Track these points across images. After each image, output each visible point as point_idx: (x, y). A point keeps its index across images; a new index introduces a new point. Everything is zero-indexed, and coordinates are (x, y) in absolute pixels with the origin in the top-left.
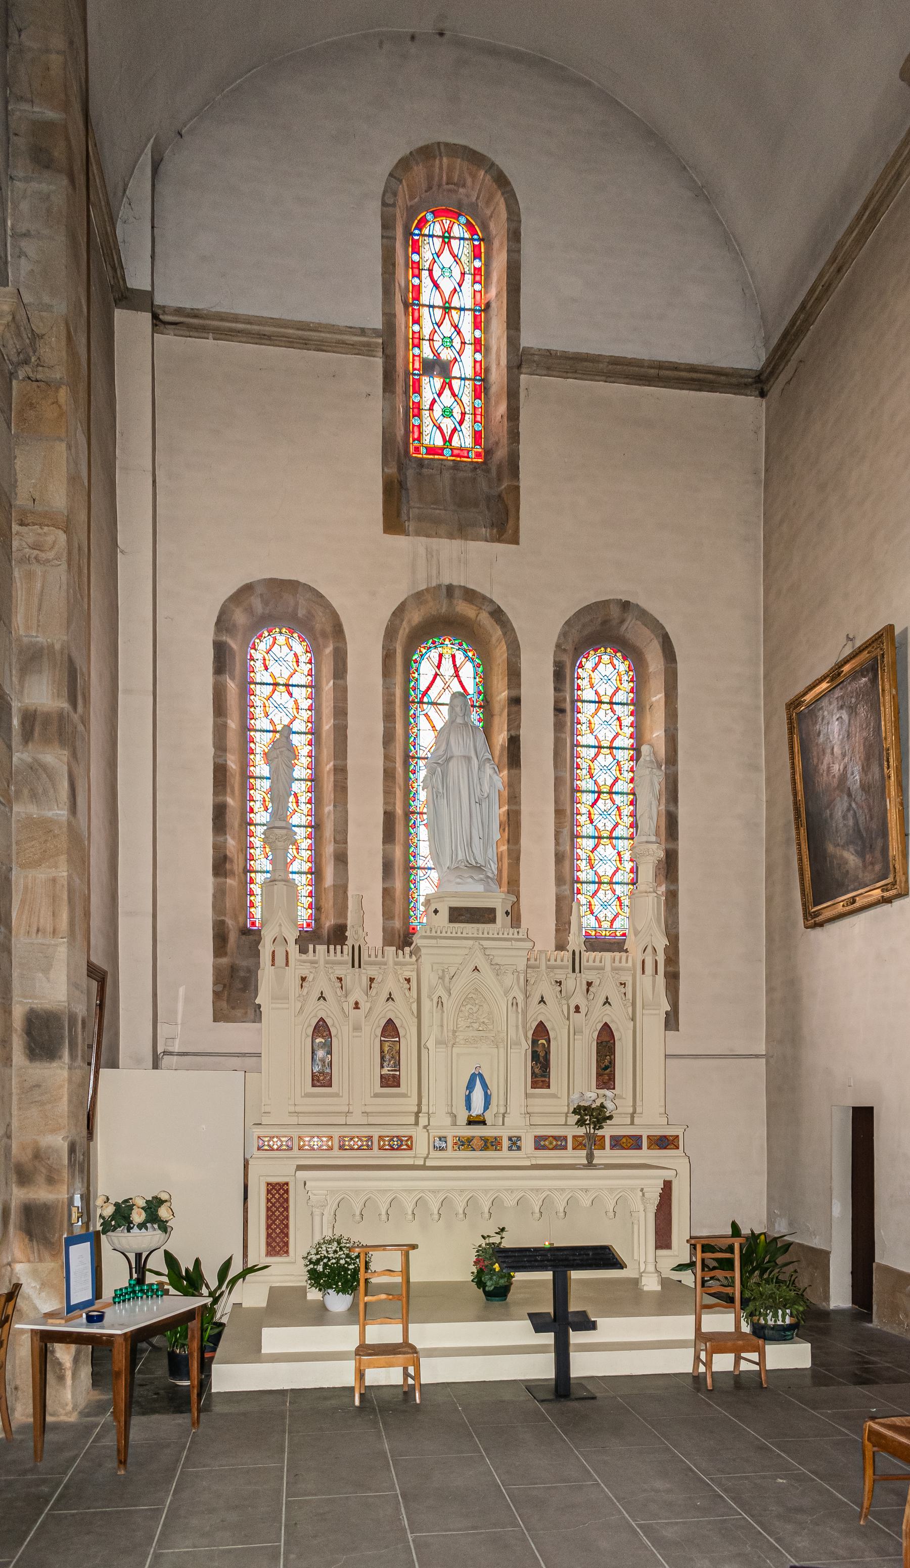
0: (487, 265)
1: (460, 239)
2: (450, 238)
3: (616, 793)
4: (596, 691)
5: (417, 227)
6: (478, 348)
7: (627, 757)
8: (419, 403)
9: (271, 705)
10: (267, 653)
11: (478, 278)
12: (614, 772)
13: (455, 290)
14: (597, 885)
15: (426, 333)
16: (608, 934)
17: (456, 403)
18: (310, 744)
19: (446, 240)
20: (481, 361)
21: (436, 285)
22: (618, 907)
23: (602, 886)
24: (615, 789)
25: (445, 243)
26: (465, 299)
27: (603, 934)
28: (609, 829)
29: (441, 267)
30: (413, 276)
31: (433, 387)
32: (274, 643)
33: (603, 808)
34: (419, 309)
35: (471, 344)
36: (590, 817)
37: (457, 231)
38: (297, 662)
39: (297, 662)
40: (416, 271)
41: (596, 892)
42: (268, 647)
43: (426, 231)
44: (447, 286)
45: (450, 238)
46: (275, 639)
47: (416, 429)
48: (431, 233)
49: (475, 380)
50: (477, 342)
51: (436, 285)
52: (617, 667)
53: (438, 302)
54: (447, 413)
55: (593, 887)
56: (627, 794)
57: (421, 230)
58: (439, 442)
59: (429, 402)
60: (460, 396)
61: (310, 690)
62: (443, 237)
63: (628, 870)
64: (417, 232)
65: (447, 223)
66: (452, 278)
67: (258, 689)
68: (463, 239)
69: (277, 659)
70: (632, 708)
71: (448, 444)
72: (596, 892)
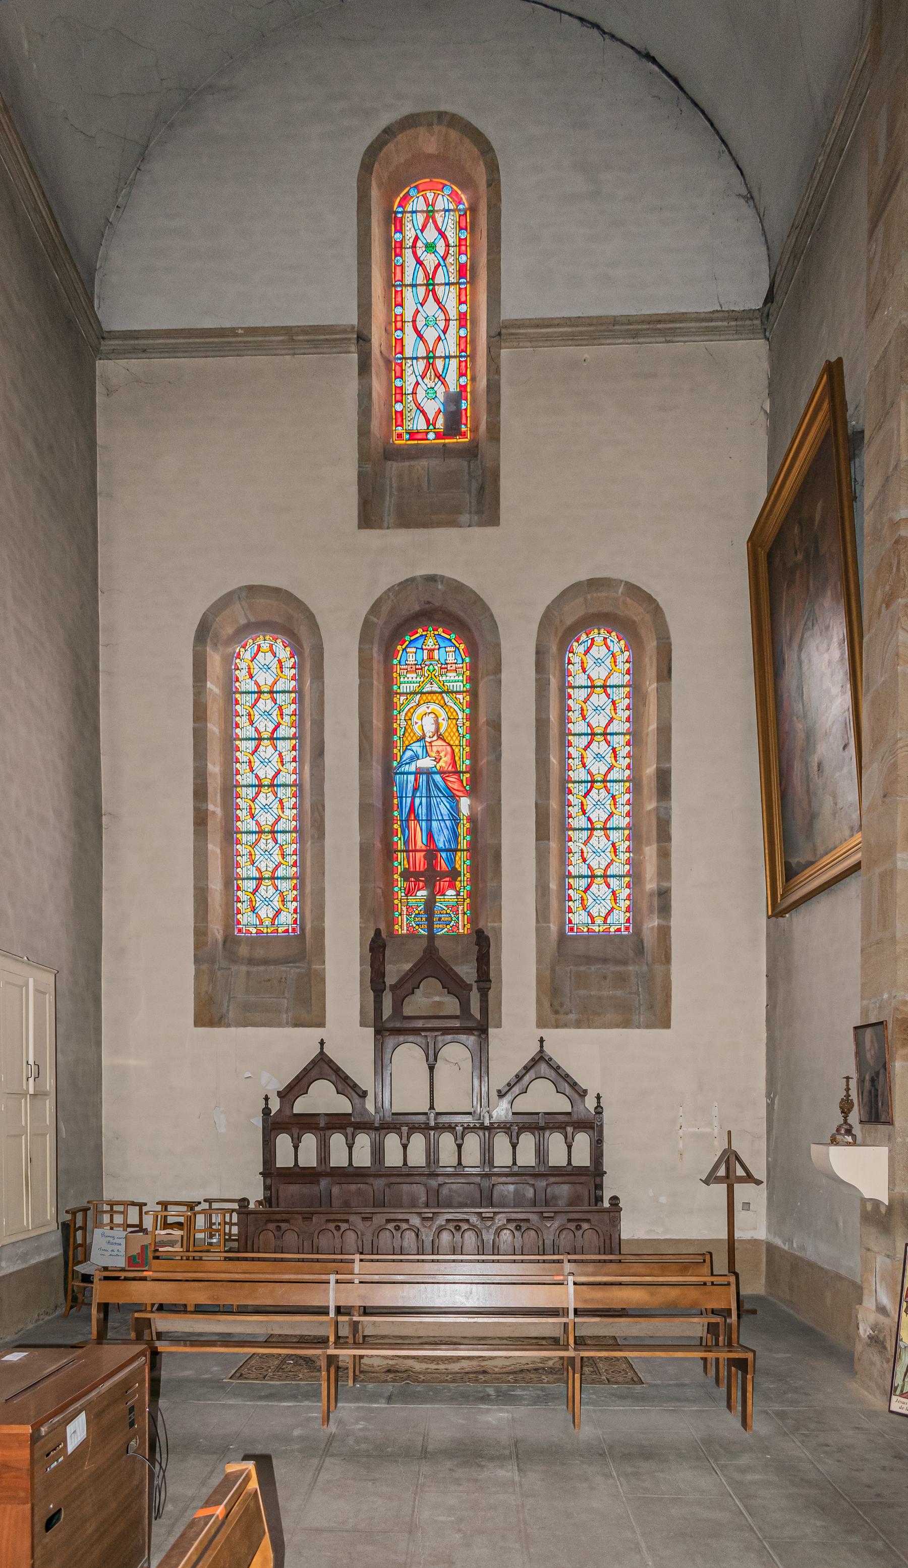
0: (473, 308)
1: (445, 211)
2: (434, 357)
3: (611, 876)
4: (588, 865)
5: (400, 205)
6: (463, 323)
7: (623, 742)
8: (401, 388)
9: (256, 666)
10: (252, 661)
11: (463, 248)
12: (608, 807)
13: (439, 338)
14: (590, 737)
15: (408, 317)
16: (601, 930)
17: (440, 310)
18: (294, 796)
19: (431, 361)
20: (466, 337)
21: (420, 335)
22: (613, 901)
23: (595, 833)
24: (610, 777)
25: (432, 352)
26: (450, 345)
27: (597, 931)
28: (603, 867)
29: (425, 327)
30: (396, 231)
31: (416, 297)
32: (258, 650)
33: (596, 798)
34: (402, 291)
35: (456, 320)
36: (582, 713)
37: (441, 203)
38: (281, 667)
39: (281, 667)
40: (398, 397)
41: (589, 887)
42: (253, 655)
43: (409, 208)
44: (430, 335)
45: (434, 285)
46: (259, 646)
47: (398, 270)
48: (414, 209)
49: (459, 283)
50: (462, 318)
51: (420, 335)
52: (611, 649)
53: (422, 352)
54: (430, 247)
55: (584, 883)
56: (624, 734)
57: (404, 207)
58: (421, 425)
59: (412, 240)
60: (443, 303)
61: (294, 789)
62: (427, 285)
63: (624, 909)
64: (400, 209)
65: (430, 196)
66: (436, 399)
67: (243, 792)
68: (449, 210)
69: (261, 667)
70: (627, 832)
71: (431, 427)
72: (589, 887)
